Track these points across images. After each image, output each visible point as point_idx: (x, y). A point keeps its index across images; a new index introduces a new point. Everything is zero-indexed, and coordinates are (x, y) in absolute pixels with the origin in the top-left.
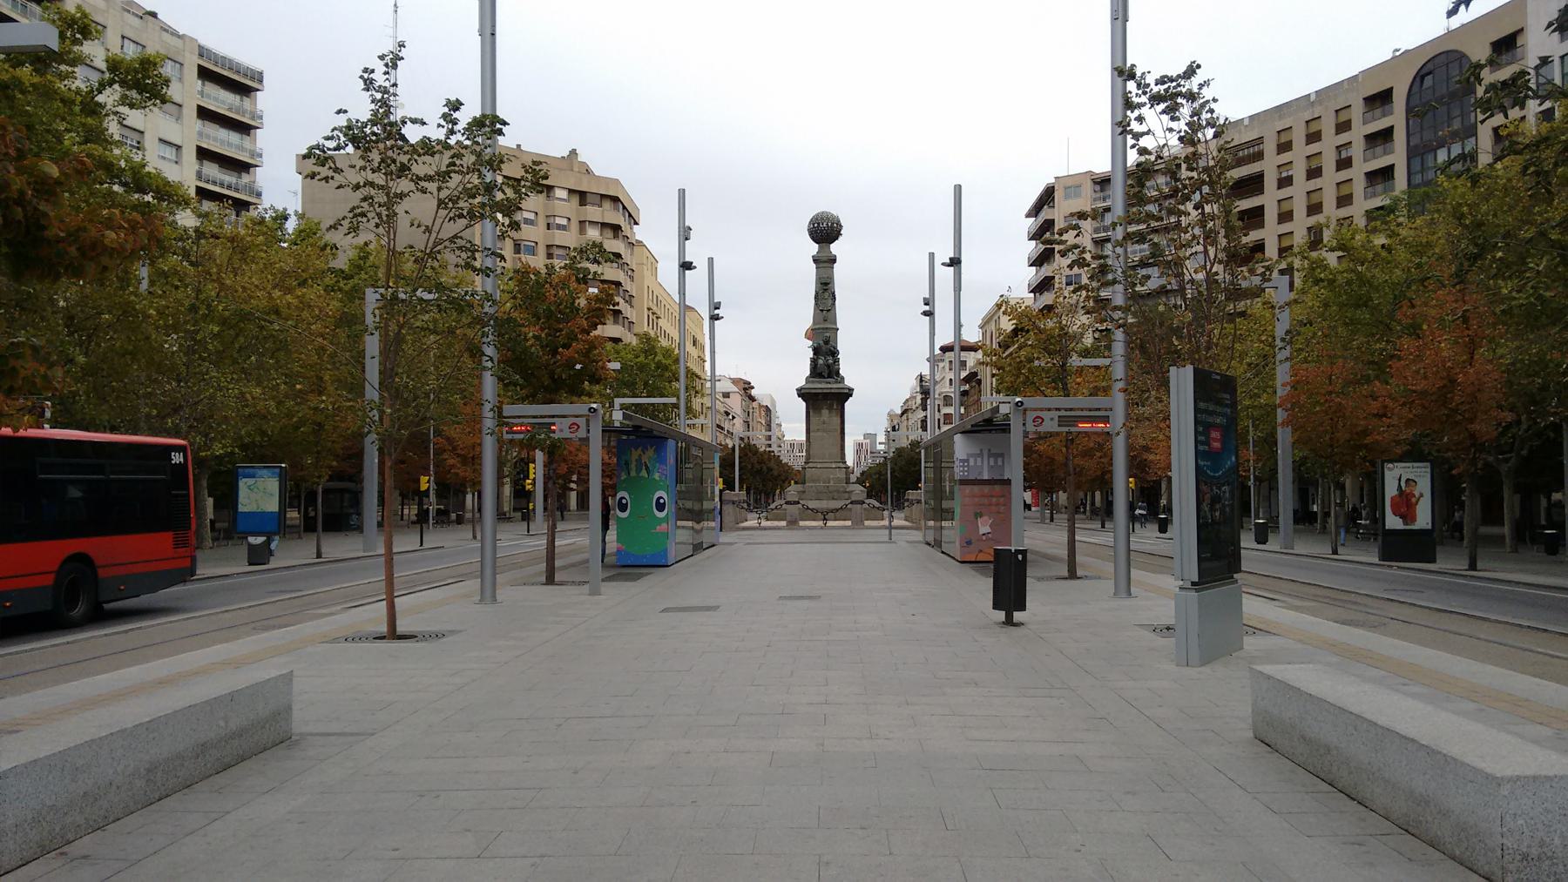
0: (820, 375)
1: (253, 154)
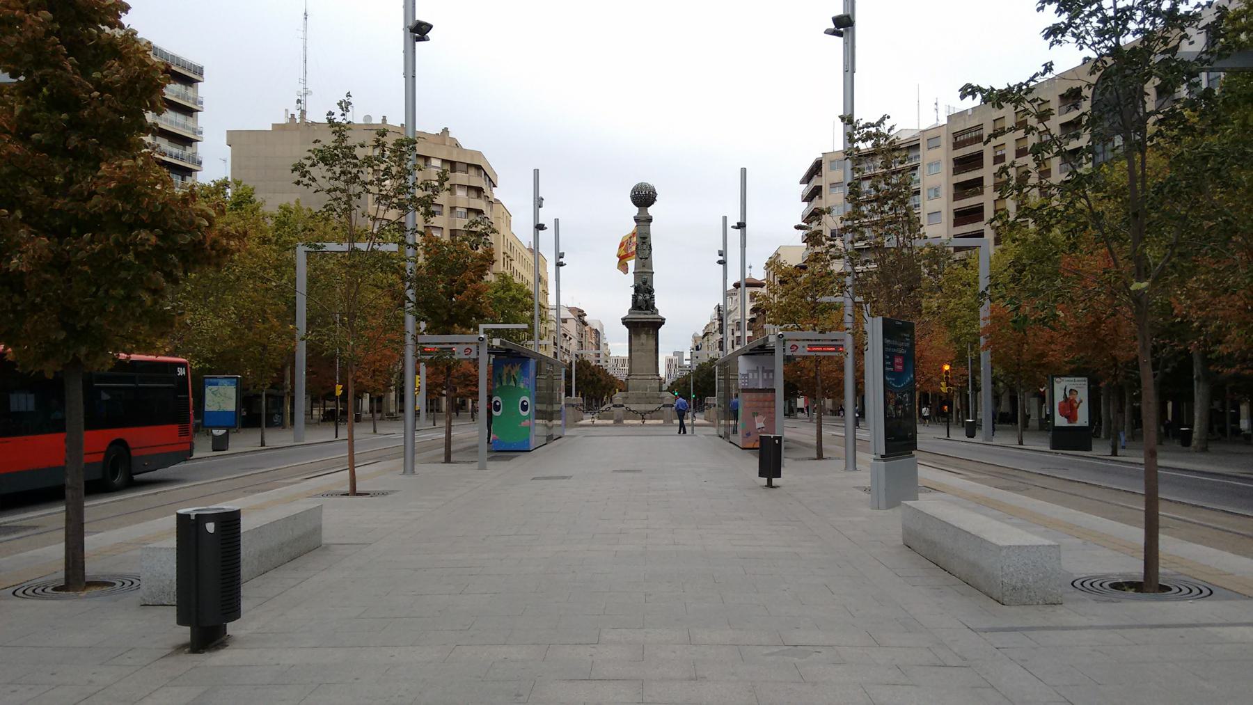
0: (640, 308)
1: (195, 131)
